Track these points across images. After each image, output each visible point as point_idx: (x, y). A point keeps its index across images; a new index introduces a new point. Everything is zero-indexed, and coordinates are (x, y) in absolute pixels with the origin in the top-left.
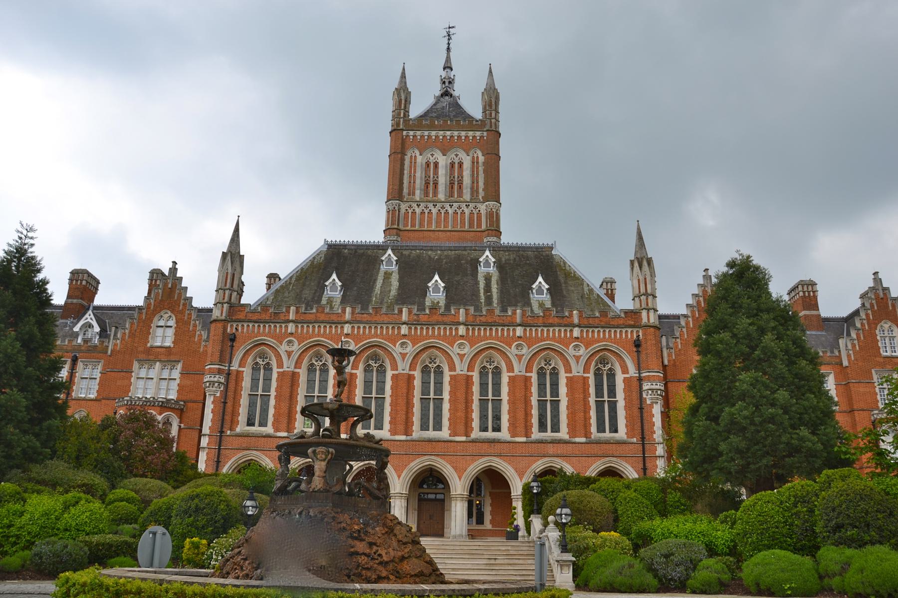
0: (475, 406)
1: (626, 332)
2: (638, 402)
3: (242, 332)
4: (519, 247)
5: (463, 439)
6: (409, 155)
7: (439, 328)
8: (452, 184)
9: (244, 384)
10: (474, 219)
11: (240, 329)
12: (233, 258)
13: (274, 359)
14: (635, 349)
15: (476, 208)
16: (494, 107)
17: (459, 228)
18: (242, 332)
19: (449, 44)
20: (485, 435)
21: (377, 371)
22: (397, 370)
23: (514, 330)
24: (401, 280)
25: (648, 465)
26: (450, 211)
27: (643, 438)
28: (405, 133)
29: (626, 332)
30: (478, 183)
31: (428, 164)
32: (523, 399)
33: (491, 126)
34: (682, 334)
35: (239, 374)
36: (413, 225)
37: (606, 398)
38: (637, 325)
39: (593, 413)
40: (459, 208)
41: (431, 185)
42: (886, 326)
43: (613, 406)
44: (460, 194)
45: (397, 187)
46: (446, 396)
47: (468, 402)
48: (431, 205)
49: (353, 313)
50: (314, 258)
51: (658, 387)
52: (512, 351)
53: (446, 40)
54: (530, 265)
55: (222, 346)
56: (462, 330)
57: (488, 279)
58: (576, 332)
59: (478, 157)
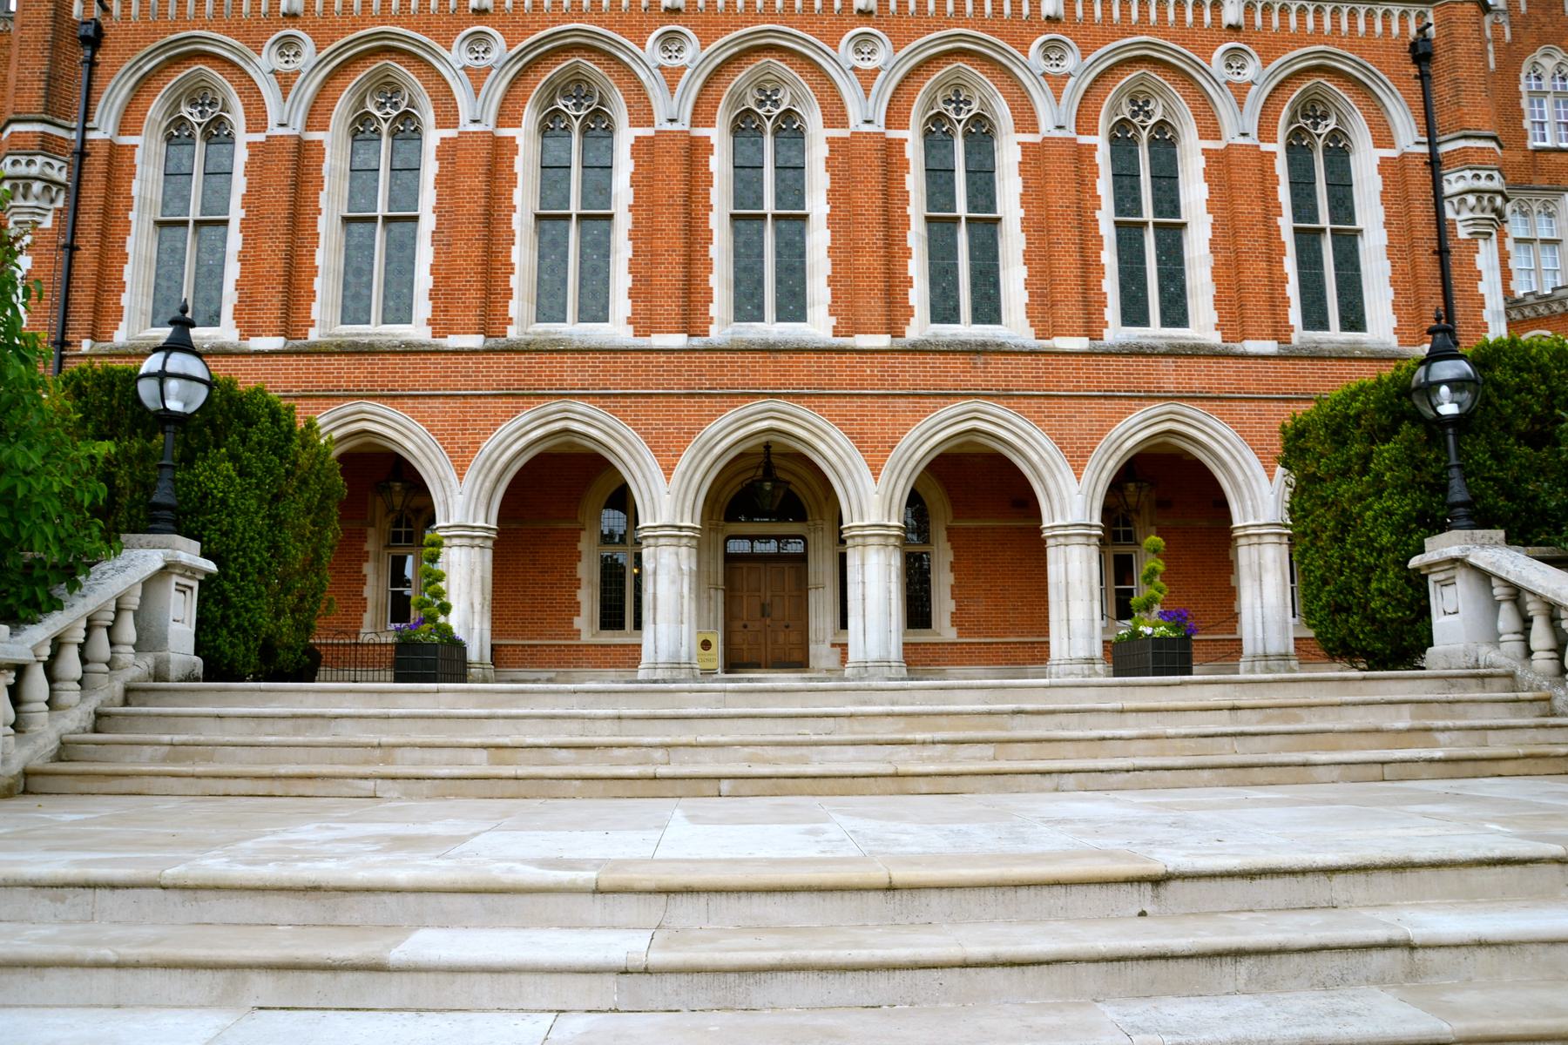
0: (916, 237)
1: (1387, 14)
2: (1432, 232)
3: (126, 17)
9: (136, 187)
14: (1414, 71)
18: (126, 17)
20: (947, 331)
22: (651, 123)
35: (118, 161)
46: (817, 205)
47: (893, 225)
55: (54, 62)
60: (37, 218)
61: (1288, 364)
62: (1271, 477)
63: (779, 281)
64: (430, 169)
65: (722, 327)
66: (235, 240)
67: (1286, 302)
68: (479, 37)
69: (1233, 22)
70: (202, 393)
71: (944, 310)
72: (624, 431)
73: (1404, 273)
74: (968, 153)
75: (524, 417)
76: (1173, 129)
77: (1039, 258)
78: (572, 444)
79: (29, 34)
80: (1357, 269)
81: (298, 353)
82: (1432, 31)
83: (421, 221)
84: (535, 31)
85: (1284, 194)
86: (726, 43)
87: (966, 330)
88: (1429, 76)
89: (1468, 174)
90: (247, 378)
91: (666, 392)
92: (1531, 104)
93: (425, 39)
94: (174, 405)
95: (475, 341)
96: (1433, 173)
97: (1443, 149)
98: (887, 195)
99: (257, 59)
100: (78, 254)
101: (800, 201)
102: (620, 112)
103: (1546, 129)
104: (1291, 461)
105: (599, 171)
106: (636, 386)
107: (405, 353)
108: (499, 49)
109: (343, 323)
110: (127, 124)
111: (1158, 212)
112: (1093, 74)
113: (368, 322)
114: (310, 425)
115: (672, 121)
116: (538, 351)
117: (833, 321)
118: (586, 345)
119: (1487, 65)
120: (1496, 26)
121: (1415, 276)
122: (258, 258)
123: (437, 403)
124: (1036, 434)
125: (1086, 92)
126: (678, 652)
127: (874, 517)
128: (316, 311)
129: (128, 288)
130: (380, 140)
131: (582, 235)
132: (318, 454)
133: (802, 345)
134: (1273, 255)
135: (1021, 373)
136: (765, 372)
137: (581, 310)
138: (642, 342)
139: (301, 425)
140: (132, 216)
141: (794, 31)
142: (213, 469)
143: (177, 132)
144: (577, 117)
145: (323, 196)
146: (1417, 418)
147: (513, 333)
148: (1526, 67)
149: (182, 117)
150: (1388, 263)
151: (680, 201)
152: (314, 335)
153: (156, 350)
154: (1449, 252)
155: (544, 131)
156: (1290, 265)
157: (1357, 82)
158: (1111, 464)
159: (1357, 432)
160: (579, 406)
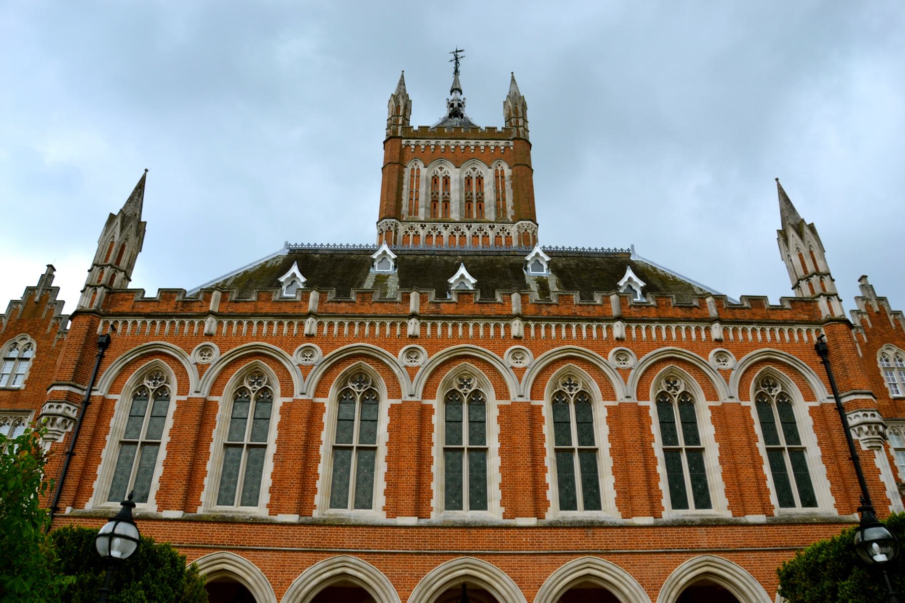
0: (550, 460)
3: (123, 334)
4: (580, 253)
6: (409, 168)
8: (469, 201)
9: (112, 423)
11: (119, 328)
12: (127, 228)
13: (174, 380)
14: (819, 359)
16: (521, 114)
18: (123, 334)
20: (570, 515)
22: (400, 397)
26: (468, 234)
28: (404, 142)
30: (504, 200)
31: (435, 179)
32: (638, 444)
35: (106, 406)
38: (814, 321)
40: (481, 229)
45: (393, 203)
46: (493, 443)
47: (536, 454)
49: (321, 301)
50: (267, 262)
53: (453, 64)
55: (82, 355)
59: (502, 171)
60: (55, 437)
61: (774, 528)
62: (773, 599)
63: (471, 487)
64: (276, 418)
65: (438, 513)
66: (162, 454)
67: (767, 491)
68: (308, 349)
69: (718, 338)
70: (133, 547)
71: (567, 503)
72: (378, 575)
73: (834, 472)
74: (577, 412)
75: (319, 565)
76: (691, 396)
77: (621, 471)
78: (347, 582)
79: (73, 341)
80: (806, 470)
81: (190, 521)
82: (825, 338)
83: (268, 447)
84: (338, 346)
85: (758, 429)
87: (580, 514)
88: (828, 362)
89: (861, 414)
90: (160, 537)
92: (886, 374)
93: (279, 349)
94: (115, 554)
95: (293, 518)
96: (840, 414)
97: (844, 400)
98: (532, 436)
99: (188, 357)
100: (74, 458)
101: (483, 441)
102: (383, 390)
103: (900, 387)
104: (787, 592)
105: (370, 423)
106: (387, 548)
107: (252, 523)
108: (319, 355)
109: (218, 504)
110: (114, 388)
111: (687, 442)
112: (644, 368)
113: (233, 505)
114: (194, 568)
115: (411, 396)
116: (330, 525)
117: (503, 509)
118: (358, 523)
119: (858, 354)
120: (858, 334)
121: (841, 473)
122: (174, 465)
123: (268, 554)
124: (626, 576)
125: (641, 377)
128: (203, 497)
129: (98, 479)
130: (249, 402)
131: (359, 458)
132: (196, 587)
133: (485, 524)
134: (756, 464)
135: (615, 540)
136: (463, 540)
137: (356, 502)
138: (391, 521)
139: (188, 567)
140: (108, 438)
141: (479, 348)
142: (132, 594)
143: (140, 394)
144: (359, 393)
145: (215, 432)
146: (862, 564)
147: (316, 514)
148: (879, 356)
149: (144, 386)
150: (824, 466)
151: (415, 440)
152: (200, 511)
153: (110, 520)
154: (858, 458)
155: (340, 400)
156: (767, 470)
157: (790, 367)
158: (673, 594)
159: (825, 574)
160: (353, 559)
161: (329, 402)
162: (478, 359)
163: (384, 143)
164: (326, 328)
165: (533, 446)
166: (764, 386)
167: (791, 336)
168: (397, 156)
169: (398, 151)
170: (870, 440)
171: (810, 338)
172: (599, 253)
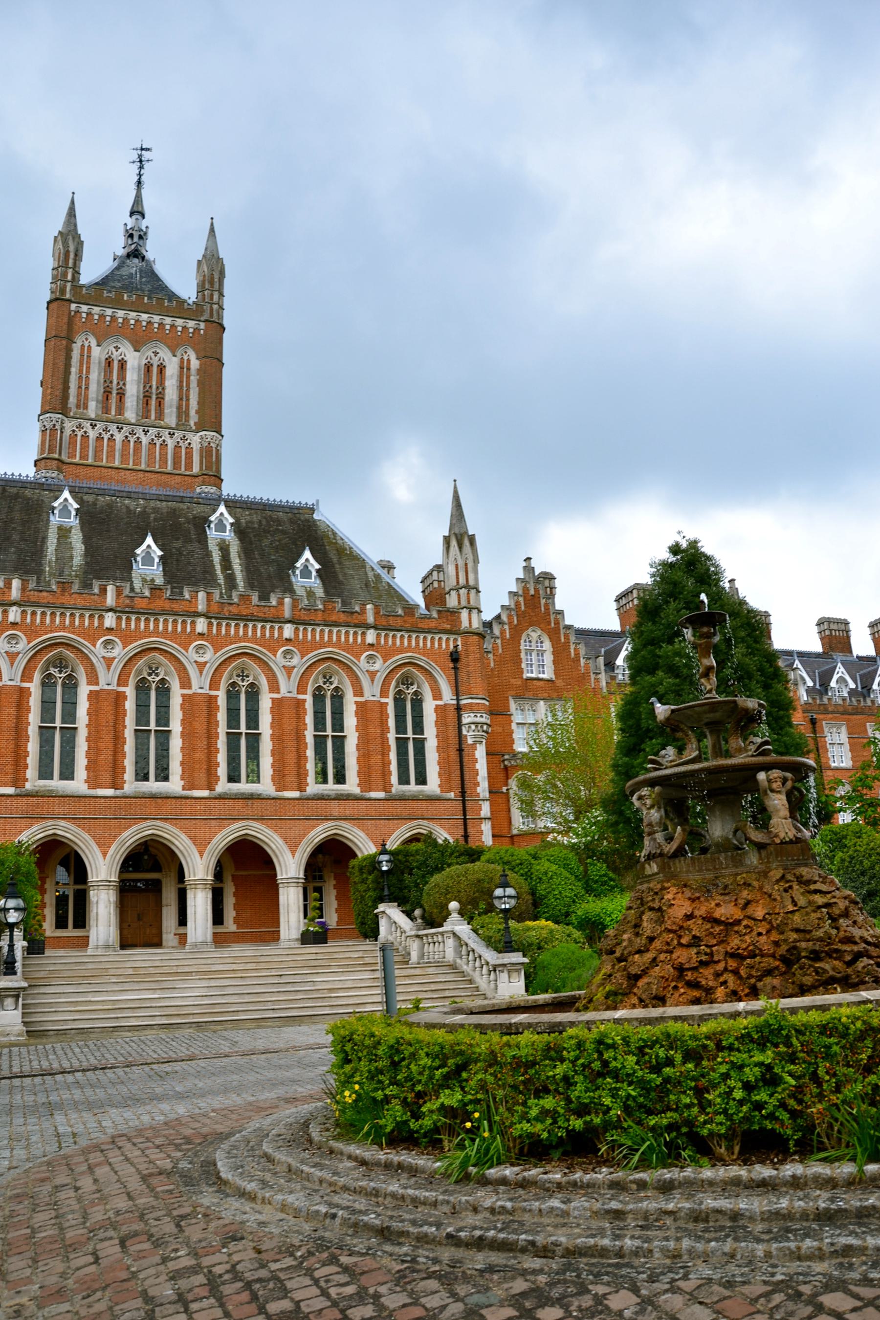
0: (222, 743)
4: (265, 505)
5: (205, 793)
7: (166, 621)
8: (147, 397)
10: (182, 455)
14: (451, 665)
15: (184, 438)
16: (216, 286)
17: (157, 468)
19: (140, 175)
20: (235, 787)
21: (64, 685)
22: (97, 684)
23: (280, 628)
24: (86, 540)
25: (471, 830)
26: (145, 440)
27: (463, 793)
28: (73, 306)
29: (440, 639)
30: (188, 400)
31: (109, 362)
33: (211, 315)
34: (495, 647)
36: (84, 456)
37: (410, 734)
39: (393, 756)
40: (159, 436)
41: (111, 395)
42: (534, 635)
43: (420, 746)
44: (160, 415)
45: (58, 393)
46: (176, 726)
47: (211, 737)
48: (113, 428)
49: (24, 589)
51: (483, 720)
52: (278, 661)
54: (284, 532)
56: (201, 625)
57: (224, 548)
58: (371, 636)
59: (189, 360)
65: (131, 785)
67: (390, 773)
68: (13, 637)
74: (247, 701)
75: (35, 828)
77: (278, 754)
84: (41, 635)
86: (134, 647)
91: (102, 817)
97: (463, 702)
108: (22, 645)
117: (182, 783)
126: (108, 940)
127: (200, 875)
131: (62, 737)
136: (150, 807)
147: (28, 786)
155: (43, 684)
160: (62, 823)
161: (34, 687)
162: (166, 651)
163: (48, 303)
164: (29, 617)
165: (209, 731)
166: (403, 684)
167: (432, 643)
168: (65, 327)
169: (66, 319)
170: (475, 736)
171: (447, 645)
172: (283, 507)
